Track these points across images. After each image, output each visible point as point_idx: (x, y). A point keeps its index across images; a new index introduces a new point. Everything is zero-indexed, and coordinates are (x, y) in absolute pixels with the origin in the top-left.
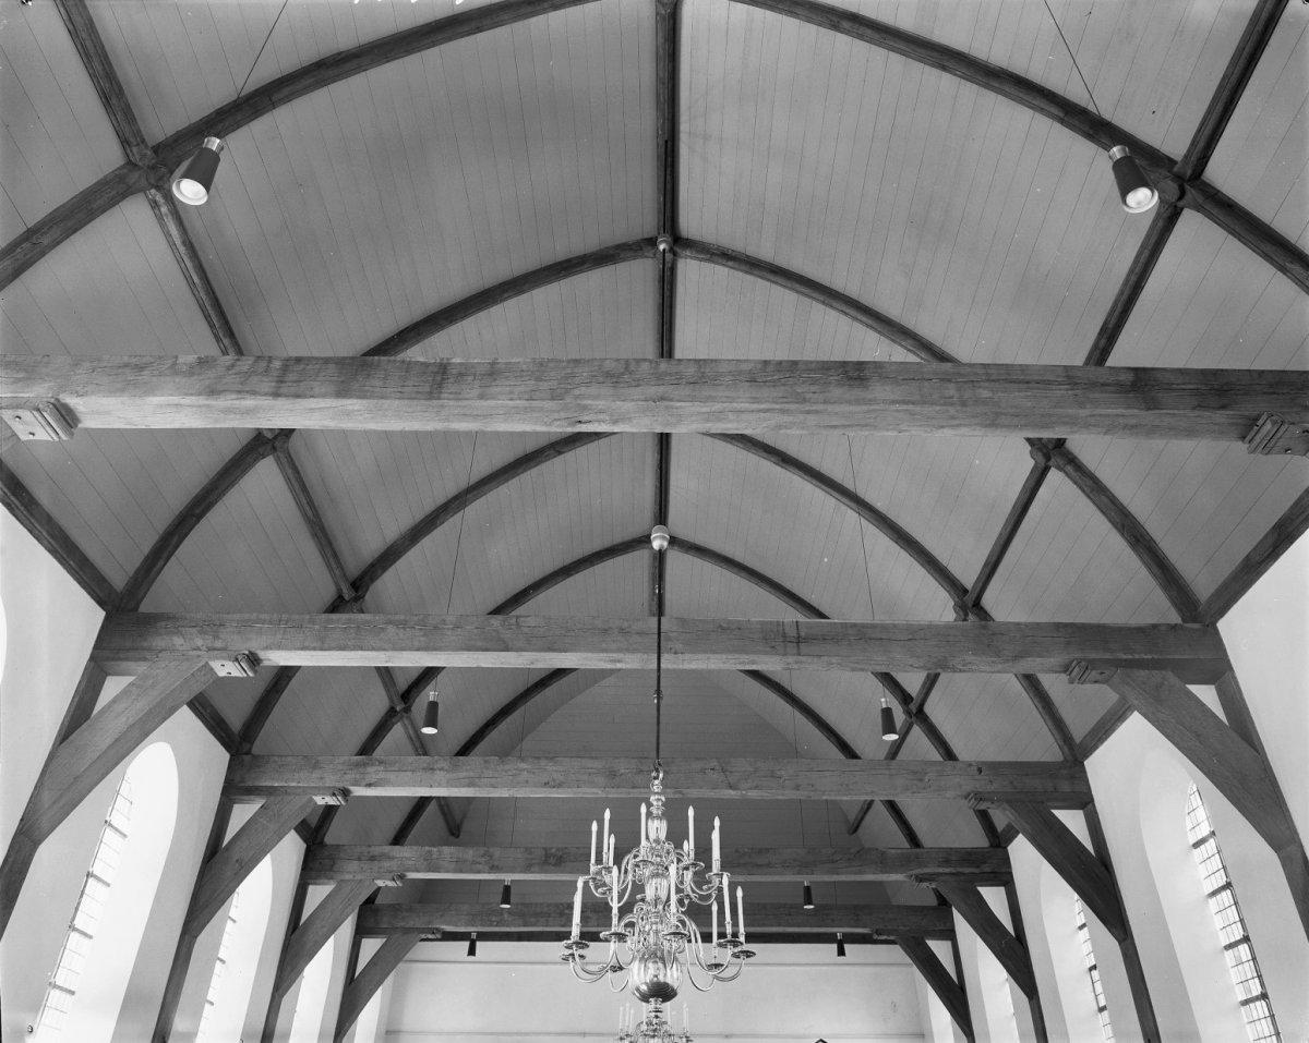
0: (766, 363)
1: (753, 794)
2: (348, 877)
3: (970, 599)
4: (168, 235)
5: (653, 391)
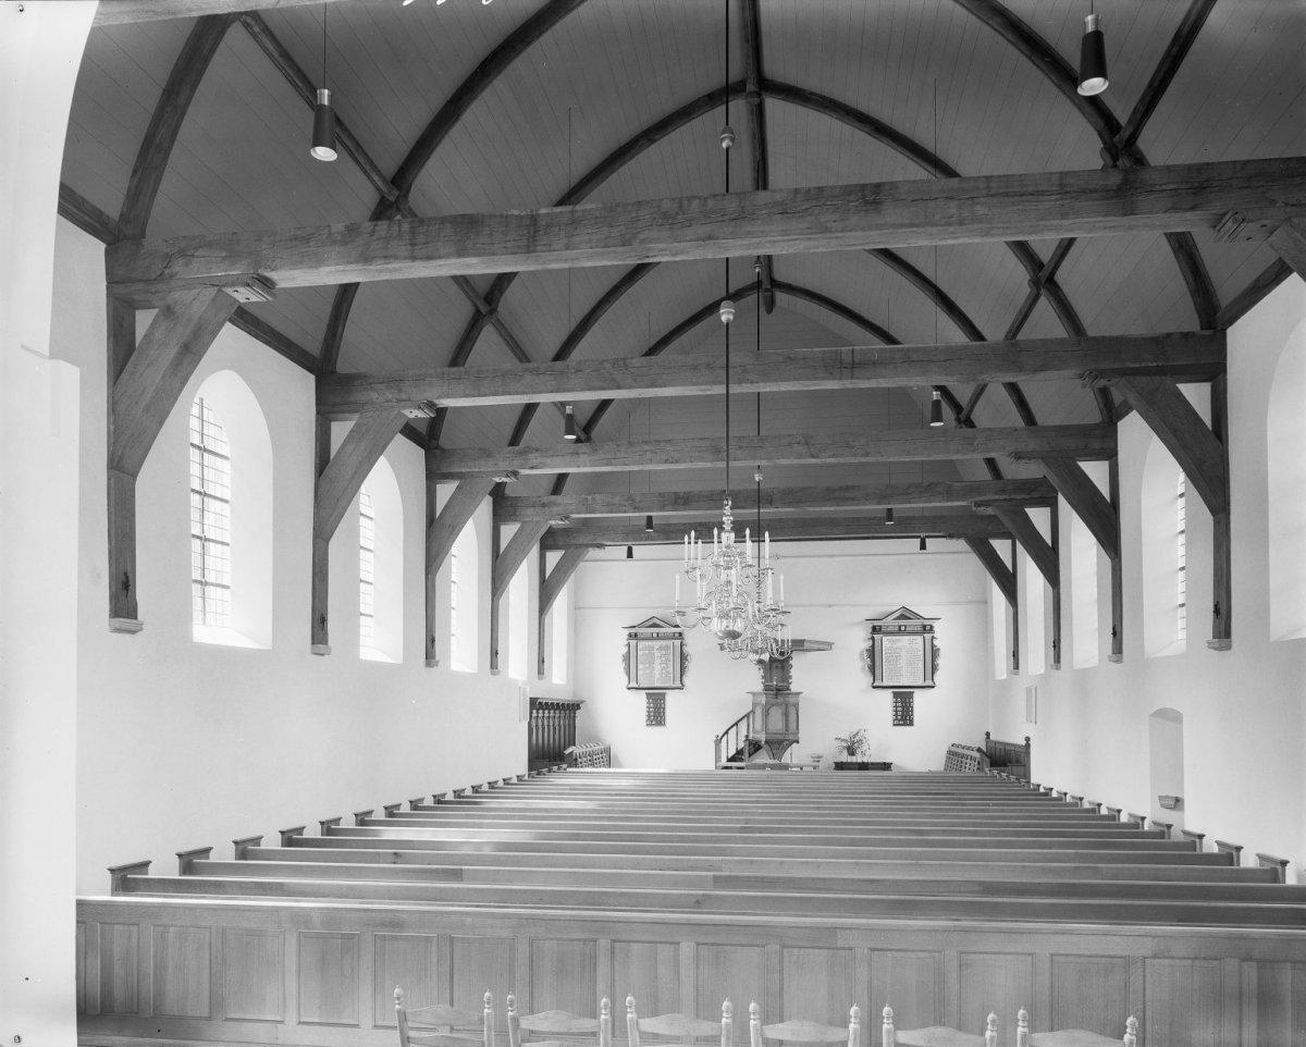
0: (796, 191)
1: (828, 460)
2: (527, 519)
3: (1044, 275)
4: (265, 49)
5: (702, 230)
